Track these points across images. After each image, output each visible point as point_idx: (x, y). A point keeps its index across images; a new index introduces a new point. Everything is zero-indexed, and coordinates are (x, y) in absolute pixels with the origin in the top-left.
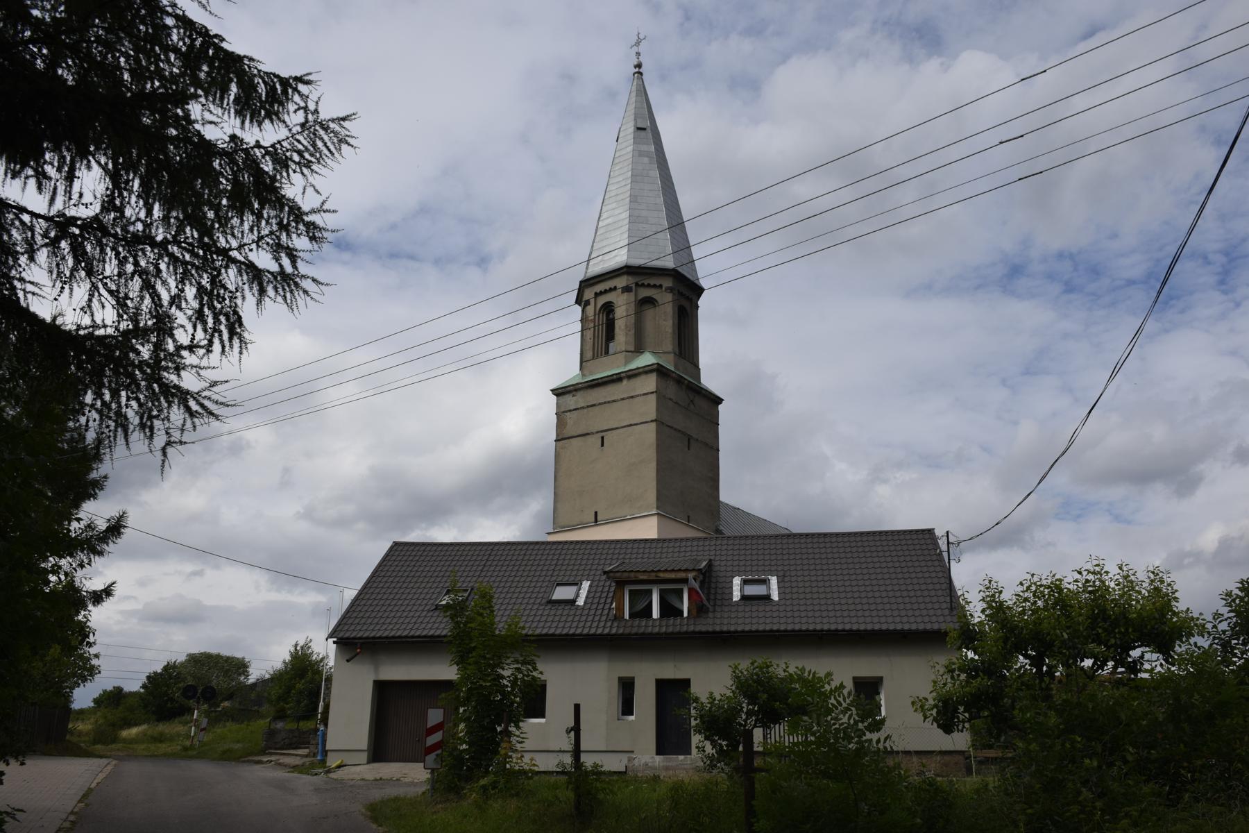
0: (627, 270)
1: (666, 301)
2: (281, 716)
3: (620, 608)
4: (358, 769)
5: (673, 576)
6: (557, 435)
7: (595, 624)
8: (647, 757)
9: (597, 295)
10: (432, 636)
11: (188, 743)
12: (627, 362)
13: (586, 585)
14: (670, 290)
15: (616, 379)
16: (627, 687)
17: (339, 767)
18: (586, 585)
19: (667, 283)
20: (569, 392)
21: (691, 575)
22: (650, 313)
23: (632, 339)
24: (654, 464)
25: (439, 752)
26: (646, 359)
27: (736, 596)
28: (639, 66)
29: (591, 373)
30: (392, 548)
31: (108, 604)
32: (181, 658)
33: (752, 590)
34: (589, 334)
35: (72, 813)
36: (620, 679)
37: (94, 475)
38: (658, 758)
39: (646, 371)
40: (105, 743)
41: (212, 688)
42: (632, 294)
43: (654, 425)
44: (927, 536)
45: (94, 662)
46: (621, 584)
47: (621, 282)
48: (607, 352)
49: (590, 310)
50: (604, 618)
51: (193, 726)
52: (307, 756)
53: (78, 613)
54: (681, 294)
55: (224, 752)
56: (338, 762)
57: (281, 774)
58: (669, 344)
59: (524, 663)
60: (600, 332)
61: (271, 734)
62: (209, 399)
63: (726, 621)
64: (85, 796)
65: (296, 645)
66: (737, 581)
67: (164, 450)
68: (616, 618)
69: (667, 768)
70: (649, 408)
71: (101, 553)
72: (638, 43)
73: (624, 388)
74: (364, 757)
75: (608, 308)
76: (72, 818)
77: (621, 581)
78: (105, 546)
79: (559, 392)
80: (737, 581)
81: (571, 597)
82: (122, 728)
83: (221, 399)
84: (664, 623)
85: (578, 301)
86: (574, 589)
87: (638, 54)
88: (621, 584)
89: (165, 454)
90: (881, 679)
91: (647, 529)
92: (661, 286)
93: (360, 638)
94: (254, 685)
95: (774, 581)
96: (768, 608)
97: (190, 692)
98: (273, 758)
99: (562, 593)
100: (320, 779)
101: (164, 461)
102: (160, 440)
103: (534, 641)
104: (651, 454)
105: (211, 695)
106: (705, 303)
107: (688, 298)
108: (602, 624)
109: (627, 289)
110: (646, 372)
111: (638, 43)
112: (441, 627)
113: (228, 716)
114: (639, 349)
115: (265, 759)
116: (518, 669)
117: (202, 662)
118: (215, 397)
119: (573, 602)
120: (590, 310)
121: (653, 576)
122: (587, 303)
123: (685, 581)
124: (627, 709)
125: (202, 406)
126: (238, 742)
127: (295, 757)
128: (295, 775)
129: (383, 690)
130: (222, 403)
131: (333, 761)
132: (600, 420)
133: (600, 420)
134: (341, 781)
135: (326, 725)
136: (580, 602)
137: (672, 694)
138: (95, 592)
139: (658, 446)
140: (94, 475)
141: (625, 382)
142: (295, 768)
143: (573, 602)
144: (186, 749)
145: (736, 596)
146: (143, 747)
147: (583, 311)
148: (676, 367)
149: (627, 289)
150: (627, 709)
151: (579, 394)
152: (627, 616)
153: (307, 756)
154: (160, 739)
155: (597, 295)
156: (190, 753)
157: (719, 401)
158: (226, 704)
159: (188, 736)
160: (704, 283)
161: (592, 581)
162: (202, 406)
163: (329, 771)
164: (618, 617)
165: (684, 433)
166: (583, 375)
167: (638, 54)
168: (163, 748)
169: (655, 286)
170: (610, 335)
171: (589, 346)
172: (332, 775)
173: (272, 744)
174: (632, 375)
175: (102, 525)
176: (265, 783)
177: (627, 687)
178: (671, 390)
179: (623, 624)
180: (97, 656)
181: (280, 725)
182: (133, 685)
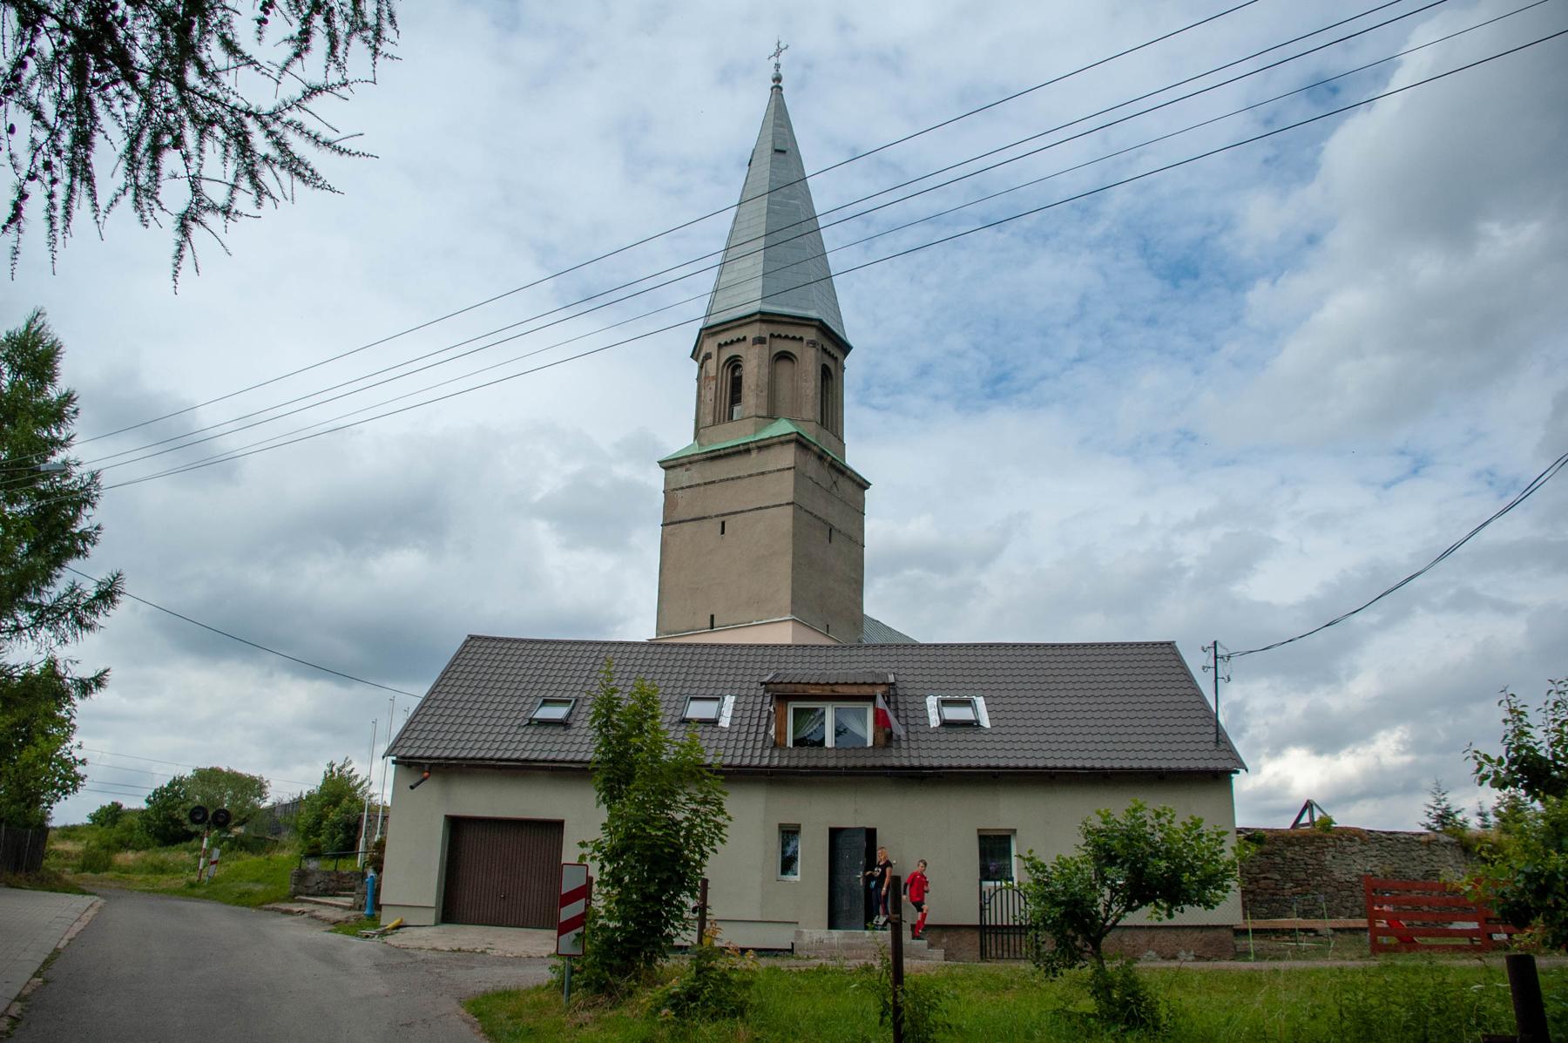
0: (765, 318)
1: (809, 360)
2: (314, 853)
3: (781, 732)
4: (424, 931)
5: (854, 691)
6: (665, 518)
7: (739, 752)
8: (815, 931)
9: (720, 346)
10: (526, 760)
11: (194, 878)
12: (756, 432)
13: (730, 701)
14: (813, 344)
15: (745, 450)
16: (789, 833)
17: (398, 927)
18: (730, 701)
19: (810, 334)
20: (682, 465)
21: (879, 691)
22: (784, 367)
23: (764, 401)
24: (789, 558)
25: (580, 930)
26: (783, 427)
27: (934, 721)
28: (778, 79)
29: (711, 442)
30: (466, 642)
31: (98, 696)
32: (188, 773)
33: (952, 713)
34: (709, 395)
35: (19, 998)
36: (780, 826)
37: (82, 525)
38: (836, 933)
39: (782, 441)
40: (95, 871)
41: (224, 811)
42: (766, 346)
43: (790, 509)
44: (1168, 650)
45: (79, 769)
46: (782, 699)
47: (752, 332)
48: (731, 418)
49: (711, 365)
50: (759, 745)
51: (202, 857)
52: (350, 908)
53: (60, 707)
54: (824, 350)
55: (242, 895)
56: (396, 922)
57: (319, 935)
58: (810, 410)
59: (704, 802)
60: (724, 389)
61: (302, 876)
62: (299, 128)
63: (914, 753)
64: (47, 963)
65: (332, 765)
66: (932, 702)
67: (185, 222)
68: (776, 745)
69: (849, 947)
70: (784, 487)
71: (89, 627)
72: (777, 54)
73: (753, 462)
74: (431, 916)
75: (734, 363)
76: (16, 1009)
77: (781, 694)
78: (94, 618)
79: (669, 465)
80: (932, 702)
81: (712, 716)
82: (118, 851)
83: (327, 134)
84: (795, 753)
85: (695, 355)
86: (715, 705)
87: (778, 66)
88: (782, 699)
89: (184, 229)
90: (1014, 831)
91: (783, 634)
92: (801, 339)
93: (429, 758)
94: (272, 810)
95: (980, 702)
96: (978, 738)
97: (198, 814)
98: (307, 907)
99: (696, 710)
100: (373, 945)
101: (181, 247)
102: (175, 195)
103: (718, 772)
104: (786, 544)
105: (222, 820)
106: (853, 368)
107: (831, 356)
108: (758, 753)
109: (760, 341)
110: (782, 443)
111: (777, 54)
112: (583, 745)
113: (241, 844)
114: (772, 416)
115: (296, 908)
116: (695, 811)
117: (209, 777)
118: (312, 125)
119: (715, 722)
120: (711, 365)
121: (827, 691)
122: (708, 356)
123: (872, 698)
124: (788, 864)
125: (280, 145)
126: (258, 881)
127: (337, 907)
128: (339, 936)
129: (457, 826)
130: (327, 144)
131: (388, 919)
132: (719, 500)
133: (719, 500)
134: (402, 950)
135: (379, 870)
136: (725, 722)
137: (853, 851)
138: (81, 680)
139: (794, 535)
140: (82, 525)
141: (754, 454)
142: (337, 925)
143: (715, 722)
144: (192, 885)
145: (934, 721)
146: (140, 877)
147: (701, 367)
148: (817, 437)
149: (760, 341)
150: (788, 864)
151: (695, 468)
152: (790, 744)
153: (350, 908)
154: (160, 869)
155: (720, 346)
156: (198, 891)
157: (863, 485)
158: (239, 830)
159: (195, 869)
160: (850, 340)
161: (738, 696)
162: (280, 145)
163: (383, 934)
164: (778, 745)
165: (825, 522)
166: (701, 445)
167: (778, 66)
168: (165, 880)
169: (794, 338)
170: (736, 394)
171: (708, 408)
172: (389, 939)
173: (303, 887)
174: (764, 446)
175: (91, 590)
176: (294, 944)
177: (789, 833)
178: (812, 467)
179: (786, 753)
180: (83, 762)
181: (313, 864)
182: (135, 802)
